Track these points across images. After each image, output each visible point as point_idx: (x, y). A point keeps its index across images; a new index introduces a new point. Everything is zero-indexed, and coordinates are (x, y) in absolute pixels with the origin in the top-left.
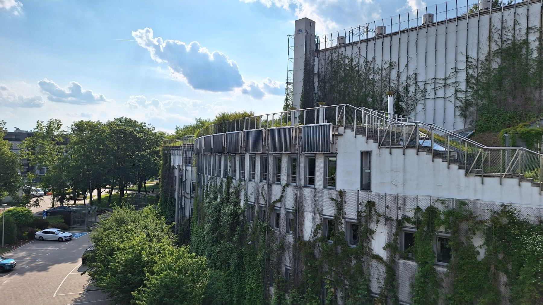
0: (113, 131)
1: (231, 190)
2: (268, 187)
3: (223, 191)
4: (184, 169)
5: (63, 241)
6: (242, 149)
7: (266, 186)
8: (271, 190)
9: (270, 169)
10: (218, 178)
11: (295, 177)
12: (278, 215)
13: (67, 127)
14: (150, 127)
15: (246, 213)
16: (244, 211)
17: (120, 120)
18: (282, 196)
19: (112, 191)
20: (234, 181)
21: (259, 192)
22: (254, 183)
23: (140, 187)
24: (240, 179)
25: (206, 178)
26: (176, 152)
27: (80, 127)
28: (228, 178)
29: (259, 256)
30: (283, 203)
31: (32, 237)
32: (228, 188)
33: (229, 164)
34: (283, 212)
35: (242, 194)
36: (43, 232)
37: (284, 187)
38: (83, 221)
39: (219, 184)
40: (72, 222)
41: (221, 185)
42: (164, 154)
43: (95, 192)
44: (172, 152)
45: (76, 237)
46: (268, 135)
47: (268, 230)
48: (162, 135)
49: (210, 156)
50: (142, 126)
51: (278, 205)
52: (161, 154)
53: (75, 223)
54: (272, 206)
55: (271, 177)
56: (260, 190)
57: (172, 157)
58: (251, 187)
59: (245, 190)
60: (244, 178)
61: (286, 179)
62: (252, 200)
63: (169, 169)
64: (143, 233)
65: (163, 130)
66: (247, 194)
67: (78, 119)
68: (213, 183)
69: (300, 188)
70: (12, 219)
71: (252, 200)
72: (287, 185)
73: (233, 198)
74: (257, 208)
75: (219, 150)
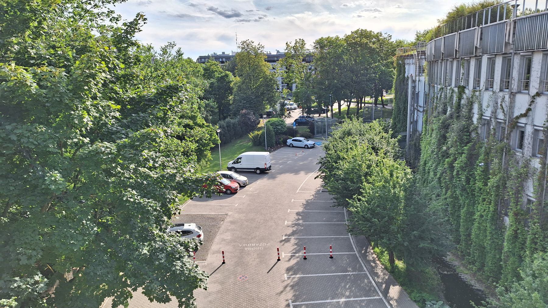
0: (349, 45)
1: (463, 102)
2: (510, 97)
3: (454, 102)
4: (417, 79)
5: (308, 148)
6: (478, 51)
7: (507, 97)
8: (514, 101)
9: (515, 74)
10: (449, 88)
11: (527, 79)
12: (522, 134)
13: (310, 46)
14: (386, 36)
15: (479, 129)
16: (477, 127)
17: (356, 32)
18: (529, 110)
19: (350, 104)
20: (467, 91)
21: (497, 103)
22: (527, 96)
23: (376, 100)
24: (474, 88)
25: (436, 88)
26: (411, 61)
27: (321, 44)
28: (459, 87)
29: (493, 181)
30: (530, 118)
31: (284, 144)
32: (460, 99)
33: (462, 71)
34: (529, 130)
35: (476, 107)
36: (293, 140)
37: (533, 97)
38: (325, 132)
39: (448, 95)
40: (316, 131)
41: (452, 97)
42: (398, 64)
43: (336, 106)
44: (407, 61)
45: (319, 145)
46: (514, 28)
47: (507, 151)
48: (400, 44)
49: (441, 63)
50: (377, 36)
51: (523, 120)
52: (395, 65)
53: (318, 133)
54: (514, 123)
55: (515, 86)
56: (499, 101)
57: (406, 67)
58: (486, 97)
59: (479, 102)
60: (479, 87)
61: (537, 86)
62: (488, 114)
63: (403, 81)
64: (368, 146)
65: (401, 38)
66: (481, 107)
67: (318, 37)
68: (443, 94)
69: (513, 95)
70: (271, 128)
71: (488, 114)
72: (538, 94)
73: (464, 111)
74: (493, 123)
75: (450, 55)
